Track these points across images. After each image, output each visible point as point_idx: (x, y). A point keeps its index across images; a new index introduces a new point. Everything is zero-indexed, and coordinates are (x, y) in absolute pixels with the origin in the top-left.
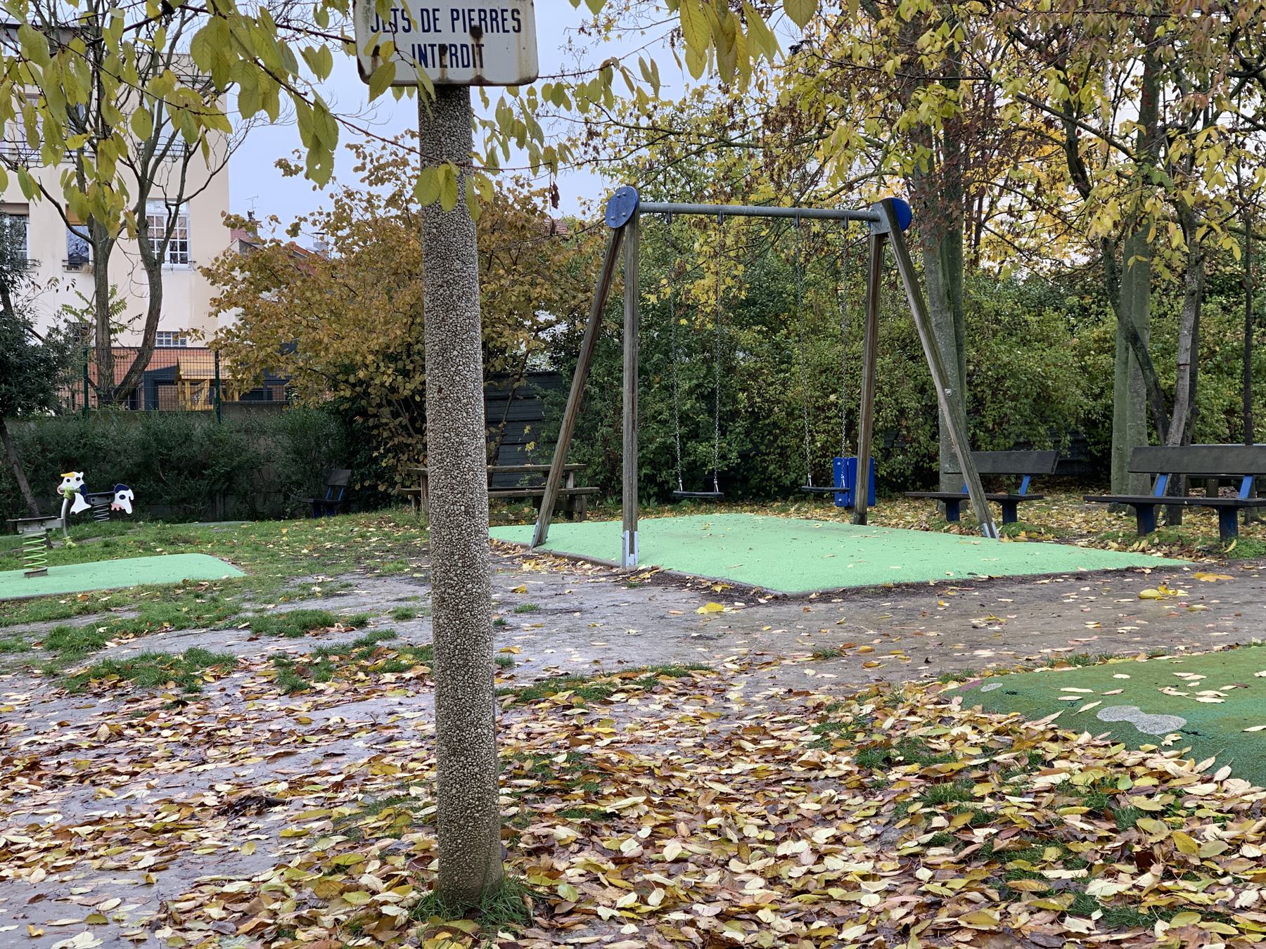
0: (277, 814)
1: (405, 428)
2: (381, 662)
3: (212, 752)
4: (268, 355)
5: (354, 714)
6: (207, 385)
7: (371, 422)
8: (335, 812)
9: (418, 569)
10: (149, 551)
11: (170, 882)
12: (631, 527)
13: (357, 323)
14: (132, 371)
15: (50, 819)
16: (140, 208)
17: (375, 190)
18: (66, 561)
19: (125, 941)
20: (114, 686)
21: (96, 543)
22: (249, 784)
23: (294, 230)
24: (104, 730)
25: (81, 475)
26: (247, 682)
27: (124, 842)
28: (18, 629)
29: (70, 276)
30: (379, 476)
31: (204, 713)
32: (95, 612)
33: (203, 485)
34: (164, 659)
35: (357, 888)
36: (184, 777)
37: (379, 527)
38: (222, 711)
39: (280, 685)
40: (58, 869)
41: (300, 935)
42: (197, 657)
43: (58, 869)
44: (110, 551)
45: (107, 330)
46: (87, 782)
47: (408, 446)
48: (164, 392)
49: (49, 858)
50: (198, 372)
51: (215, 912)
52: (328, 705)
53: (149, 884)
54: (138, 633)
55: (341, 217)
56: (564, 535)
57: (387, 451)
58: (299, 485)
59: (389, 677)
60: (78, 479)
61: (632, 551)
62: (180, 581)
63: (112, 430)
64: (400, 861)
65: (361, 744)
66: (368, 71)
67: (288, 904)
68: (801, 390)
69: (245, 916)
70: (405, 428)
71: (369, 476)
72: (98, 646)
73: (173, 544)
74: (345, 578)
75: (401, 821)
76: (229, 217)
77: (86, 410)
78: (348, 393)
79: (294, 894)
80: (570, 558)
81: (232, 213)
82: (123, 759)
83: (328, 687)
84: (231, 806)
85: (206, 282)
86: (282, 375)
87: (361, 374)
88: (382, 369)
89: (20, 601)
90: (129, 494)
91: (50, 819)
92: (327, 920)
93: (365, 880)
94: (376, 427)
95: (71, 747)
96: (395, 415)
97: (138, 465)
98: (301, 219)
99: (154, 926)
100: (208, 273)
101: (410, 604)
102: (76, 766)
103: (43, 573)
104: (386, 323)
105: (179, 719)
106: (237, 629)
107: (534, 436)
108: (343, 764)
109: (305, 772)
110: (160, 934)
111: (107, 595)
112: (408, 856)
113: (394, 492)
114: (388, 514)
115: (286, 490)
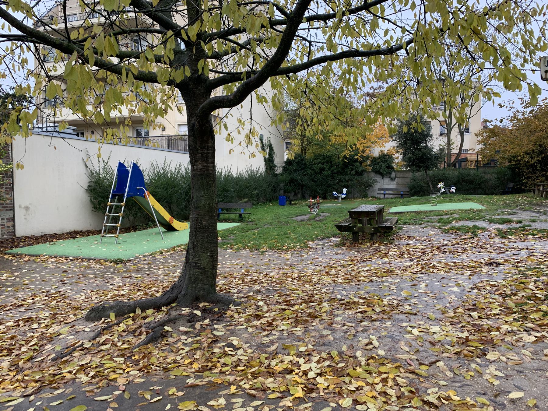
0: (501, 267)
1: (531, 172)
2: (527, 233)
3: (482, 250)
5: (521, 245)
8: (519, 269)
9: (536, 209)
10: (460, 201)
11: (475, 279)
13: (518, 144)
15: (443, 261)
17: (525, 110)
18: (441, 203)
19: (466, 291)
20: (455, 232)
21: (447, 199)
22: (493, 259)
23: (501, 121)
24: (454, 242)
26: (489, 234)
27: (462, 268)
28: (431, 217)
29: (441, 137)
30: (523, 185)
31: (479, 240)
34: (467, 227)
35: (528, 289)
36: (475, 255)
37: (522, 198)
38: (484, 241)
39: (498, 236)
40: (447, 272)
41: (512, 297)
42: (475, 227)
43: (447, 272)
44: (451, 201)
45: (449, 149)
47: (531, 177)
48: (463, 164)
49: (444, 269)
51: (488, 288)
52: (513, 242)
53: (470, 279)
54: (460, 220)
55: (515, 117)
57: (525, 178)
58: (498, 186)
59: (530, 236)
63: (451, 173)
64: (540, 284)
65: (524, 253)
66: (544, 77)
67: (508, 289)
69: (496, 290)
71: (519, 185)
72: (451, 223)
73: (466, 200)
74: (514, 210)
75: (539, 274)
77: (444, 168)
78: (514, 163)
79: (509, 287)
82: (460, 249)
83: (513, 238)
84: (489, 263)
85: (476, 137)
86: (495, 159)
87: (519, 158)
90: (455, 188)
91: (443, 261)
92: (520, 295)
93: (530, 287)
95: (446, 245)
99: (472, 289)
100: (476, 135)
101: (534, 218)
102: (448, 249)
103: (436, 205)
104: (527, 144)
105: (473, 241)
108: (519, 257)
109: (508, 258)
110: (474, 291)
112: (542, 283)
114: (525, 195)
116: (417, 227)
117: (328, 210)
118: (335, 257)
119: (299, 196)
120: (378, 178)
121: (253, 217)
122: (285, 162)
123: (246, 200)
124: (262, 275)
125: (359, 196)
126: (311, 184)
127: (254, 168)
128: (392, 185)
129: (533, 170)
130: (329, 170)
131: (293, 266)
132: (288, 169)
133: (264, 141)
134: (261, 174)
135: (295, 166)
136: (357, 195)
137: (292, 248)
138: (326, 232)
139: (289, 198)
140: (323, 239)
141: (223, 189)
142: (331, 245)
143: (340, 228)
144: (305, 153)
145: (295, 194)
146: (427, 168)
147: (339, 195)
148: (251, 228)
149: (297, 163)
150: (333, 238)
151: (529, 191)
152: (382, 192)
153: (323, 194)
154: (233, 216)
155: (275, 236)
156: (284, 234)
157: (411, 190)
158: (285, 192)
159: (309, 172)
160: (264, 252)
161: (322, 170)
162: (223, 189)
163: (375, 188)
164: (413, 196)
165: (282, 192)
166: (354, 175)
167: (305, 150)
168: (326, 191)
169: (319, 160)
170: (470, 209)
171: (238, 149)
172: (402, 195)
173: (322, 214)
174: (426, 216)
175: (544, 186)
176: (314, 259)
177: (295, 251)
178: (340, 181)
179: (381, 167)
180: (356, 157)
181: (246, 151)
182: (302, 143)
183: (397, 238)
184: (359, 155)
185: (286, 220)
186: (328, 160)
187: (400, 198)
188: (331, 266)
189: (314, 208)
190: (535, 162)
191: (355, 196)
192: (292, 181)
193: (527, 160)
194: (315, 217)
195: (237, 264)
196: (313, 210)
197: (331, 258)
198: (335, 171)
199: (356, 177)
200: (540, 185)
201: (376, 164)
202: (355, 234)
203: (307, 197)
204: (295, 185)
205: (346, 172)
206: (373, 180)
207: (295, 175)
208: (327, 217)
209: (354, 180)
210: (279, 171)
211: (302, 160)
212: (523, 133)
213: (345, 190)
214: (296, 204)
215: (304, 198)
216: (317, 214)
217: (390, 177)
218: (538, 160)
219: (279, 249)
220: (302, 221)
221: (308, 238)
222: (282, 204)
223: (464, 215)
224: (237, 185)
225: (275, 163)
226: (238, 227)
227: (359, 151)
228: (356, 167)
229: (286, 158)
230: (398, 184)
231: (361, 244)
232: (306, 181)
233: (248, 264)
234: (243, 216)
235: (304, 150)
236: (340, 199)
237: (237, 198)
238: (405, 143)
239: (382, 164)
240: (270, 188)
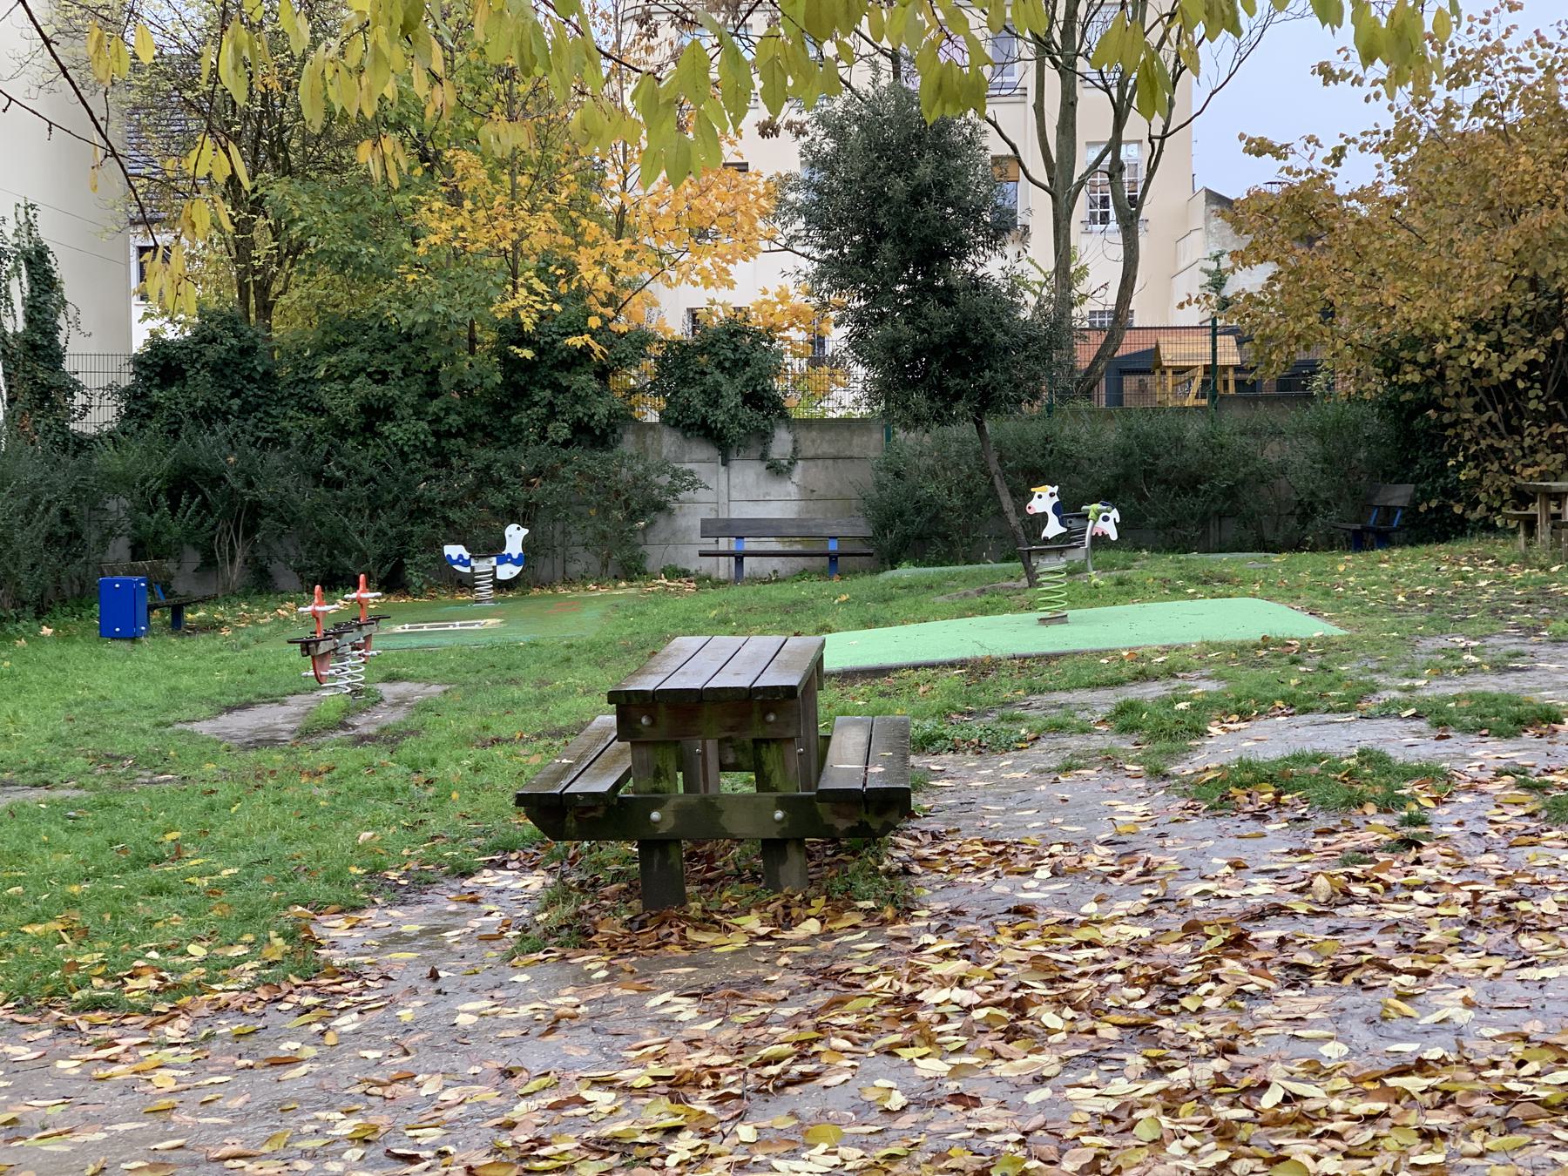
4: (1309, 327)
6: (1200, 374)
7: (1447, 418)
10: (1177, 593)
13: (1432, 278)
14: (1098, 357)
16: (1115, 144)
25: (1055, 489)
28: (1061, 697)
30: (1450, 493)
32: (1156, 679)
33: (1198, 505)
46: (1348, 981)
48: (1130, 383)
50: (1191, 356)
60: (1052, 495)
62: (1258, 638)
70: (1494, 426)
73: (1211, 584)
76: (1251, 140)
78: (1415, 377)
81: (1256, 135)
88: (1471, 343)
90: (1115, 515)
94: (1453, 425)
96: (1479, 408)
97: (1116, 478)
98: (1348, 141)
103: (1062, 619)
104: (1480, 276)
106: (1398, 716)
111: (1162, 654)
113: (1473, 516)
115: (1306, 512)
116: (1010, 768)
117: (424, 663)
118: (535, 1057)
119: (235, 573)
120: (698, 460)
122: (139, 362)
125: (596, 566)
126: (306, 497)
129: (1506, 417)
130: (418, 413)
132: (154, 407)
135: (200, 388)
137: (199, 988)
138: (434, 824)
139: (166, 588)
140: (421, 884)
144: (266, 309)
145: (209, 563)
146: (987, 402)
147: (483, 566)
149: (219, 370)
150: (488, 877)
151: (1488, 527)
152: (724, 544)
153: (384, 559)
155: (66, 879)
156: (139, 862)
157: (882, 527)
159: (295, 423)
161: (375, 413)
164: (894, 563)
165: (120, 549)
166: (566, 444)
167: (262, 289)
168: (404, 539)
169: (354, 355)
170: (1266, 643)
172: (833, 558)
173: (388, 690)
174: (1032, 690)
176: (376, 1088)
177: (222, 1009)
178: (486, 477)
183: (923, 861)
185: (150, 742)
190: (1516, 374)
191: (575, 568)
192: (747, 363)
193: (1478, 362)
194: (347, 712)
196: (331, 668)
197: (509, 1074)
198: (454, 420)
199: (576, 454)
201: (684, 381)
202: (654, 846)
203: (286, 578)
204: (205, 504)
205: (519, 430)
207: (205, 441)
208: (426, 708)
209: (565, 471)
211: (247, 351)
212: (1447, 216)
213: (515, 537)
215: (262, 584)
216: (356, 692)
217: (763, 457)
218: (1532, 364)
219: (95, 1005)
220: (264, 741)
221: (318, 889)
223: (1249, 678)
225: (67, 366)
227: (591, 300)
228: (577, 399)
230: (808, 494)
231: (706, 922)
236: (485, 590)
238: (867, 253)
240: (41, 526)
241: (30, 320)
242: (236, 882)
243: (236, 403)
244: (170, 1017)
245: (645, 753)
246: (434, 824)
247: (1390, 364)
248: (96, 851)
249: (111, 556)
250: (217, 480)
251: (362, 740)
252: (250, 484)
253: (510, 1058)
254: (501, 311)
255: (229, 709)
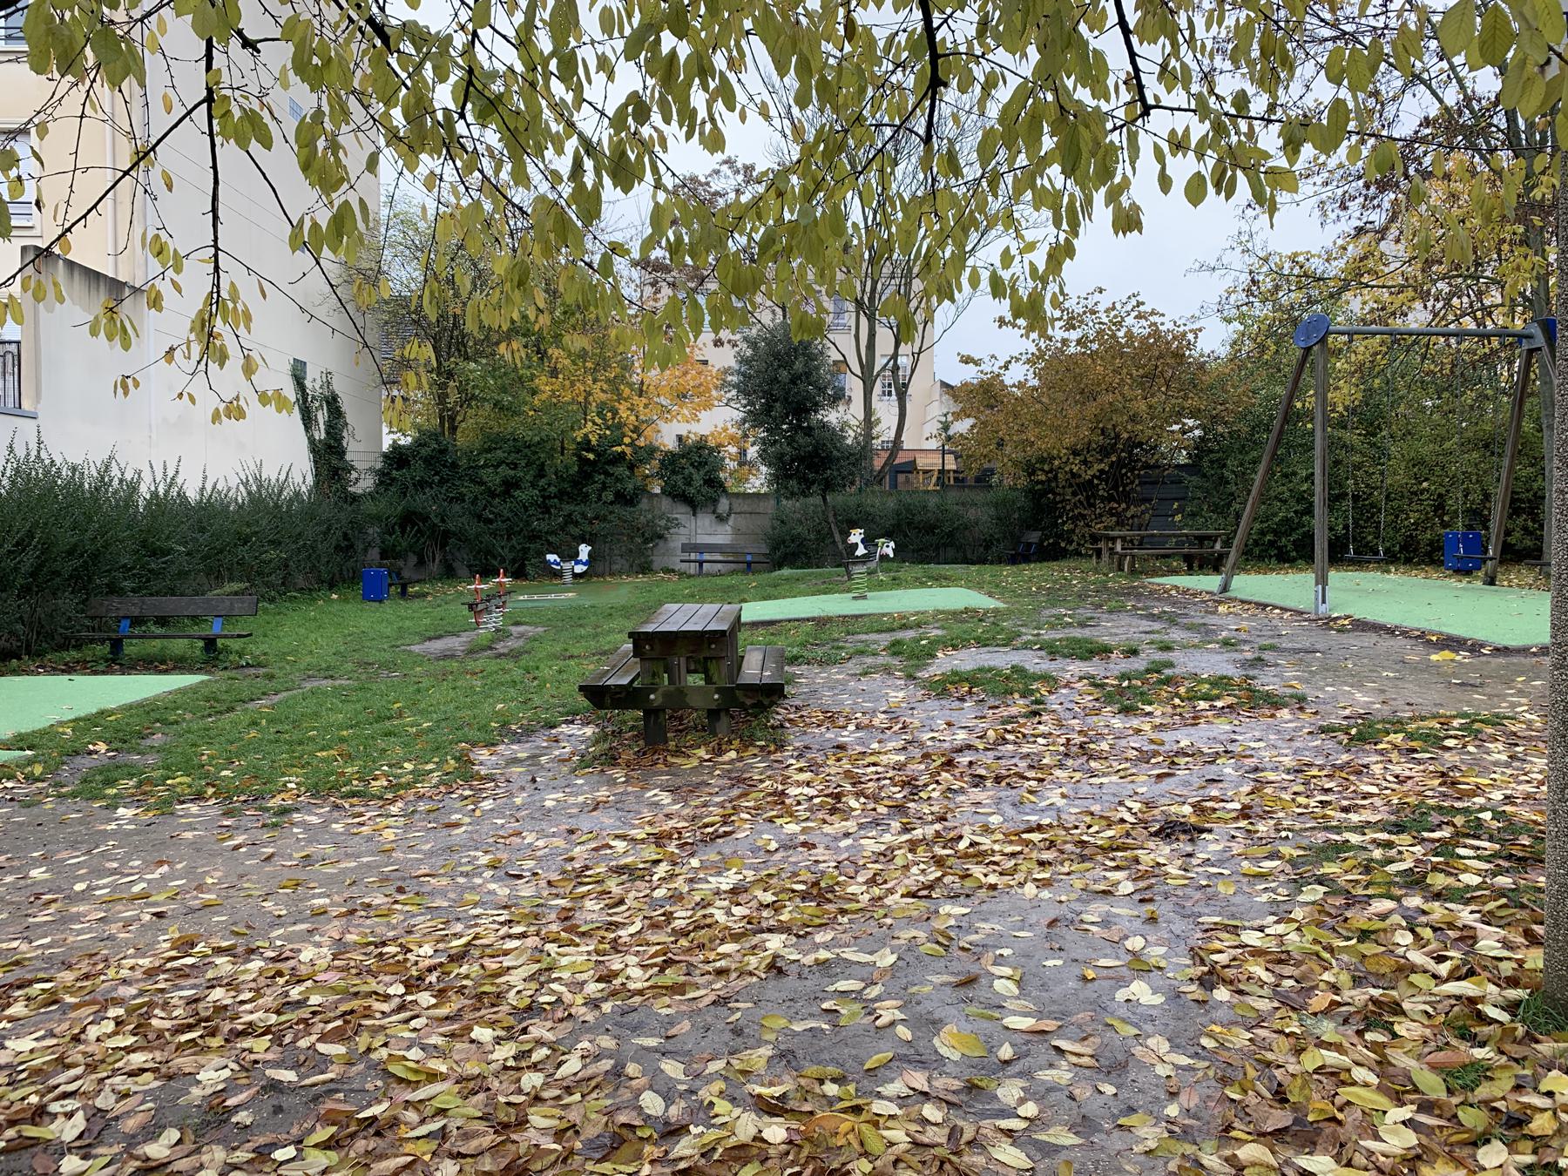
10: (923, 585)
12: (1322, 581)
28: (864, 637)
48: (901, 478)
56: (1249, 584)
61: (1324, 602)
68: (1399, 477)
73: (941, 581)
78: (1043, 478)
80: (1258, 604)
89: (857, 617)
96: (1074, 494)
103: (864, 597)
107: (1180, 510)
115: (988, 546)
116: (836, 674)
117: (535, 617)
118: (585, 823)
119: (435, 567)
120: (681, 513)
121: (256, 649)
122: (385, 456)
123: (236, 586)
124: (256, 964)
125: (627, 566)
126: (473, 528)
127: (271, 473)
128: (721, 536)
129: (1088, 498)
130: (533, 485)
131: (411, 886)
132: (393, 480)
133: (308, 383)
134: (297, 494)
135: (418, 470)
136: (619, 563)
137: (409, 786)
138: (537, 701)
139: (398, 575)
140: (528, 732)
141: (144, 544)
142: (563, 761)
143: (599, 696)
144: (453, 429)
145: (421, 562)
146: (828, 486)
147: (567, 566)
148: (244, 696)
149: (427, 461)
150: (564, 729)
152: (693, 556)
153: (514, 561)
154: (179, 646)
156: (379, 719)
157: (774, 549)
158: (384, 554)
159: (468, 489)
160: (284, 811)
161: (510, 485)
162: (144, 544)
163: (672, 545)
164: (780, 566)
165: (374, 554)
166: (612, 503)
167: (452, 419)
168: (525, 550)
169: (499, 453)
170: (966, 610)
171: (162, 381)
172: (749, 564)
173: (514, 629)
174: (848, 633)
175: (1123, 539)
176: (501, 839)
177: (421, 797)
179: (688, 481)
180: (619, 449)
181: (198, 386)
182: (442, 399)
184: (627, 440)
185: (387, 656)
186: (529, 453)
187: (745, 572)
188: (579, 876)
189: (488, 611)
190: (1094, 476)
191: (615, 567)
192: (409, 519)
194: (492, 641)
195: (144, 896)
197: (571, 832)
199: (617, 508)
200: (1114, 539)
201: (674, 472)
202: (651, 713)
204: (419, 531)
205: (587, 495)
206: (668, 520)
207: (420, 498)
209: (611, 517)
210: (364, 484)
211: (443, 451)
213: (584, 551)
214: (422, 595)
215: (449, 573)
216: (498, 630)
218: (1102, 471)
219: (353, 794)
220: (448, 656)
221: (473, 734)
222: (374, 595)
223: (957, 628)
224: (202, 530)
225: (348, 457)
226: (194, 689)
228: (617, 480)
229: (386, 445)
230: (737, 531)
231: (678, 752)
232: (459, 518)
233: (200, 888)
234: (220, 642)
235: (450, 420)
236: (568, 578)
237: (202, 578)
238: (768, 409)
239: (692, 470)
241: (328, 433)
242: (430, 730)
243: (437, 478)
244: (393, 802)
245: (647, 664)
246: (537, 701)
247: (1031, 470)
248: (357, 713)
249: (369, 557)
250: (425, 518)
251: (500, 656)
252: (443, 521)
253: (573, 823)
254: (579, 435)
255: (430, 639)
